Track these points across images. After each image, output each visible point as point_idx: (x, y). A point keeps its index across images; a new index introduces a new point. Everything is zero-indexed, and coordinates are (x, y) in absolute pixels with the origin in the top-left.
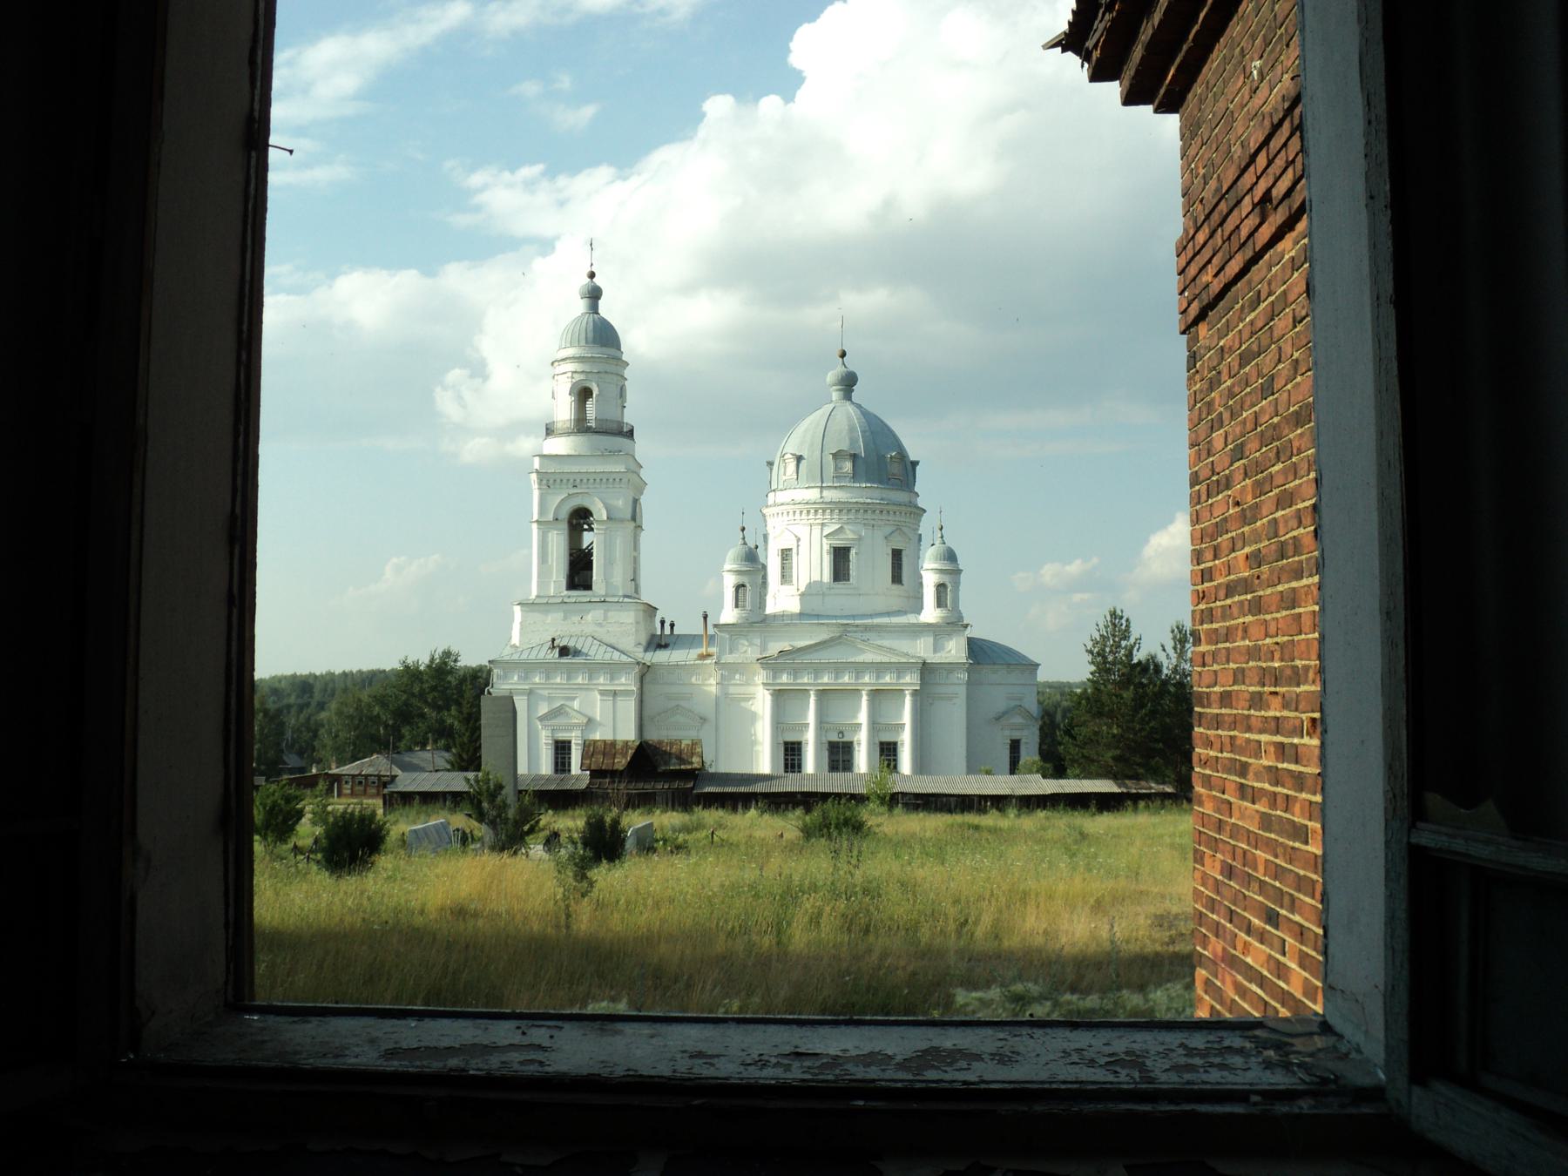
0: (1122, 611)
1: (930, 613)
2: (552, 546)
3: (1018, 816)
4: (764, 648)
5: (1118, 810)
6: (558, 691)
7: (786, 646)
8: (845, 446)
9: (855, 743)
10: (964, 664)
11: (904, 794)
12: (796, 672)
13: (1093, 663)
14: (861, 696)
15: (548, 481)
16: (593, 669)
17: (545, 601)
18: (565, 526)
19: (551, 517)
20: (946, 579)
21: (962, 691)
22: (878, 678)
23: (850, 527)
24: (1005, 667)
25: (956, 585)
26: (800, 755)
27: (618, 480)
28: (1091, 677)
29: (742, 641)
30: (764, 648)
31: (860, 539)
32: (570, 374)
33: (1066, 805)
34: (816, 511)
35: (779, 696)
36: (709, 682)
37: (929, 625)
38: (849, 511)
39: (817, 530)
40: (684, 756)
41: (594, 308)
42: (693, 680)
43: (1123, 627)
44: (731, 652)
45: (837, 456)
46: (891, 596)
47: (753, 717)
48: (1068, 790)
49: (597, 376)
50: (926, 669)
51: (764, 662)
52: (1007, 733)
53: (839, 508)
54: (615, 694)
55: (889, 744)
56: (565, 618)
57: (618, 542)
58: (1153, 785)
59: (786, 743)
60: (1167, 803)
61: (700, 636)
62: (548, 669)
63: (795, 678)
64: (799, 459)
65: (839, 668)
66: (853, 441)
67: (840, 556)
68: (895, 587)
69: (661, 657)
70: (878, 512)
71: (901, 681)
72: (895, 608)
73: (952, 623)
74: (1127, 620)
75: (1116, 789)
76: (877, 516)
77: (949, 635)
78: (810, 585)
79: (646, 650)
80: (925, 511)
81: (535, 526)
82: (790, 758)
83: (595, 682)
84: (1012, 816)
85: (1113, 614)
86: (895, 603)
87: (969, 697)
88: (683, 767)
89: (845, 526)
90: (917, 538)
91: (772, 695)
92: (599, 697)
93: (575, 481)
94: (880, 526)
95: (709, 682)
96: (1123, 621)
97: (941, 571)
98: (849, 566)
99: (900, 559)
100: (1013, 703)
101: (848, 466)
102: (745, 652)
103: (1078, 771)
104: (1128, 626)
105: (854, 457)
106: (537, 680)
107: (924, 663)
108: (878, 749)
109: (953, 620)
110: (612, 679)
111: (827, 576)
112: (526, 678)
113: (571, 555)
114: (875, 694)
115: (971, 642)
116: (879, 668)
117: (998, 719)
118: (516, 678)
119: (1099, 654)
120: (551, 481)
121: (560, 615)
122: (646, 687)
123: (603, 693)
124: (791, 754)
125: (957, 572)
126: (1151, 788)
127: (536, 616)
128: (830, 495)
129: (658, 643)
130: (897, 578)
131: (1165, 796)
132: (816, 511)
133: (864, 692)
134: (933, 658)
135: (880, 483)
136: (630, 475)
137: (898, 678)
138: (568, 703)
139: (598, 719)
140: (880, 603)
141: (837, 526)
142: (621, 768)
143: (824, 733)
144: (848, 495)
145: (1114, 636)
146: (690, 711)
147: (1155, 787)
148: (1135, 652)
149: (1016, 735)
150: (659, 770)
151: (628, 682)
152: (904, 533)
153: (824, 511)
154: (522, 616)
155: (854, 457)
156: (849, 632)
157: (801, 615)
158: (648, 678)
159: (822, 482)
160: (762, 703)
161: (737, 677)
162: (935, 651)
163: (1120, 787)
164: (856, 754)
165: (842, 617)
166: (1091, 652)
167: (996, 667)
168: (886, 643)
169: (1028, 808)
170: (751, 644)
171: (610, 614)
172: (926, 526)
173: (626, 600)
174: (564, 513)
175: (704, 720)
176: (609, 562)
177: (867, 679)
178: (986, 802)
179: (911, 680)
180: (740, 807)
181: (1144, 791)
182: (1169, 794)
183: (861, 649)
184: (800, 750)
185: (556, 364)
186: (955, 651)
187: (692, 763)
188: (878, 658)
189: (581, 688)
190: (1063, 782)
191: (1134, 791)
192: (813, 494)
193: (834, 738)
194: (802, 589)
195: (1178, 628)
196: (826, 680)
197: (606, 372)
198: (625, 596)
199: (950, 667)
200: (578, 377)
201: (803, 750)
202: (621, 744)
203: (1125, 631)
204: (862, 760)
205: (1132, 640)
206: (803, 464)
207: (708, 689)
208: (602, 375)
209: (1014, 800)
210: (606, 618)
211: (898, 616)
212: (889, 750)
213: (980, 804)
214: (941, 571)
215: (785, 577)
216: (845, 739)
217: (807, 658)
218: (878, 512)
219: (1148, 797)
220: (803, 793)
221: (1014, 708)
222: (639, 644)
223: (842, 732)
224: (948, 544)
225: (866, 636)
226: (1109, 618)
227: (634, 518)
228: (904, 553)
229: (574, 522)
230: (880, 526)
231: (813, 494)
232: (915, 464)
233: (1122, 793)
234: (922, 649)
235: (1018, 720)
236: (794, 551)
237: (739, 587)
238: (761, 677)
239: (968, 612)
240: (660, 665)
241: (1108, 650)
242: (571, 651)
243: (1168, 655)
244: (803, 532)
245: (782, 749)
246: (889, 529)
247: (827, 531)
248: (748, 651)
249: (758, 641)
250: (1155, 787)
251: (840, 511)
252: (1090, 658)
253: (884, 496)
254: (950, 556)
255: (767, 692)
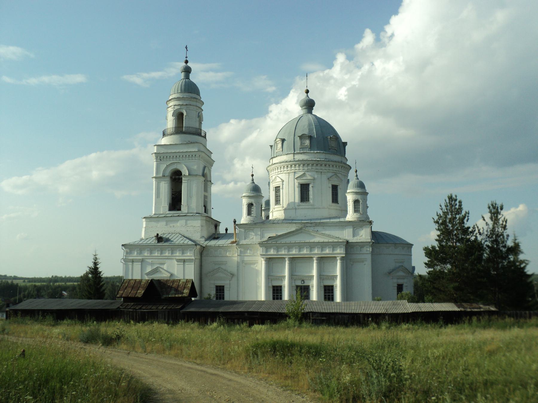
0: (456, 196)
1: (351, 216)
2: (162, 189)
3: (388, 328)
4: (262, 236)
5: (459, 323)
6: (157, 260)
7: (273, 235)
8: (306, 132)
9: (310, 286)
10: (369, 242)
11: (314, 313)
12: (278, 248)
13: (438, 230)
14: (313, 261)
15: (160, 157)
16: (174, 248)
17: (157, 216)
18: (168, 179)
19: (161, 175)
20: (359, 197)
21: (369, 257)
22: (322, 250)
23: (309, 173)
24: (393, 245)
25: (365, 200)
26: (281, 293)
27: (194, 155)
28: (438, 238)
29: (251, 233)
30: (262, 236)
31: (314, 179)
32: (173, 107)
33: (422, 320)
34: (291, 166)
35: (269, 261)
36: (234, 255)
37: (350, 222)
38: (308, 165)
39: (292, 175)
40: (179, 289)
41: (187, 77)
42: (228, 254)
43: (457, 207)
44: (245, 239)
45: (301, 137)
46: (332, 209)
47: (257, 272)
48: (423, 310)
49: (185, 107)
50: (348, 245)
51: (261, 244)
52: (395, 281)
53: (304, 163)
54: (184, 261)
55: (329, 286)
56: (167, 225)
57: (194, 186)
58: (481, 306)
59: (274, 287)
60: (494, 317)
61: (233, 234)
62: (151, 248)
63: (278, 251)
64: (283, 140)
65: (300, 246)
66: (310, 130)
67: (304, 189)
68: (334, 204)
69: (213, 243)
70: (323, 165)
71: (335, 252)
72: (334, 216)
73: (363, 221)
74: (460, 202)
75: (456, 309)
76: (323, 167)
77: (361, 227)
78: (289, 204)
79: (206, 240)
80: (413, 245)
81: (154, 180)
82: (275, 294)
83: (174, 255)
84: (384, 328)
85: (451, 198)
86: (334, 213)
87: (373, 261)
88: (177, 296)
89: (307, 173)
90: (346, 181)
91: (266, 261)
92: (176, 263)
93: (176, 156)
94: (325, 172)
95: (234, 255)
96: (457, 202)
97: (356, 193)
98: (309, 193)
99: (337, 190)
100: (398, 265)
101: (307, 142)
102: (253, 238)
103: (430, 298)
104: (460, 205)
105: (311, 138)
106: (146, 254)
107: (347, 242)
108: (323, 289)
109: (363, 219)
110: (183, 253)
111: (297, 199)
112: (141, 253)
113: (173, 194)
114: (321, 260)
115: (374, 235)
116: (323, 245)
117: (390, 273)
118: (136, 253)
119: (442, 224)
120: (162, 157)
121: (164, 223)
122: (204, 258)
123: (178, 261)
124: (277, 292)
125: (365, 194)
126: (480, 308)
127: (153, 224)
128: (298, 157)
129: (215, 236)
130: (335, 199)
131: (491, 313)
132: (291, 166)
133: (314, 259)
134: (352, 239)
135: (325, 151)
136: (200, 153)
137: (333, 250)
138: (161, 266)
139: (176, 274)
140: (325, 213)
141: (302, 173)
142: (140, 296)
143: (293, 281)
144: (308, 157)
145: (452, 212)
146: (225, 270)
147: (484, 308)
148: (465, 221)
149: (400, 282)
150: (163, 298)
151: (190, 255)
152: (339, 177)
153: (295, 165)
154: (146, 224)
155: (311, 138)
156: (307, 227)
157: (285, 219)
158: (205, 253)
159: (294, 151)
160: (261, 265)
161: (248, 251)
162: (354, 236)
163: (459, 308)
164: (311, 292)
165: (305, 220)
166: (437, 222)
167: (388, 245)
168: (327, 232)
169: (397, 322)
170: (256, 235)
171: (188, 222)
172: (351, 175)
173: (197, 215)
174: (168, 173)
175: (233, 275)
176: (189, 196)
177: (316, 251)
178: (368, 318)
179: (340, 251)
180: (209, 321)
181: (476, 310)
182: (493, 311)
183: (314, 236)
184: (281, 290)
185: (168, 103)
186: (364, 235)
187: (183, 293)
188: (322, 240)
189: (168, 258)
190: (421, 305)
191: (469, 310)
192: (290, 157)
193: (299, 283)
194: (285, 206)
195: (492, 205)
196: (294, 252)
197: (190, 105)
198: (197, 213)
199: (362, 245)
200: (177, 107)
201: (282, 290)
202: (144, 281)
203: (459, 209)
204: (314, 295)
205: (463, 213)
206: (285, 143)
207: (234, 258)
208: (187, 106)
209: (387, 317)
210: (186, 224)
211: (335, 219)
212: (329, 290)
213: (364, 319)
214: (356, 193)
215: (277, 201)
216: (305, 284)
217: (284, 241)
218: (323, 165)
219: (479, 314)
220: (248, 312)
221: (400, 266)
222: (203, 237)
223: (303, 281)
224: (360, 179)
225: (317, 228)
226: (448, 201)
227: (204, 175)
228: (339, 187)
229: (173, 177)
230: (325, 172)
231: (290, 157)
232: (345, 144)
233: (461, 311)
234: (347, 235)
235: (401, 273)
236: (281, 187)
237: (250, 206)
238: (260, 250)
239: (371, 214)
240: (210, 246)
241: (448, 221)
242: (164, 239)
243: (487, 223)
244: (284, 176)
245: (271, 290)
246: (330, 175)
247: (297, 176)
248: (254, 238)
249: (259, 233)
250: (484, 308)
251: (304, 165)
252: (436, 226)
253: (327, 157)
254: (361, 185)
255: (262, 259)
